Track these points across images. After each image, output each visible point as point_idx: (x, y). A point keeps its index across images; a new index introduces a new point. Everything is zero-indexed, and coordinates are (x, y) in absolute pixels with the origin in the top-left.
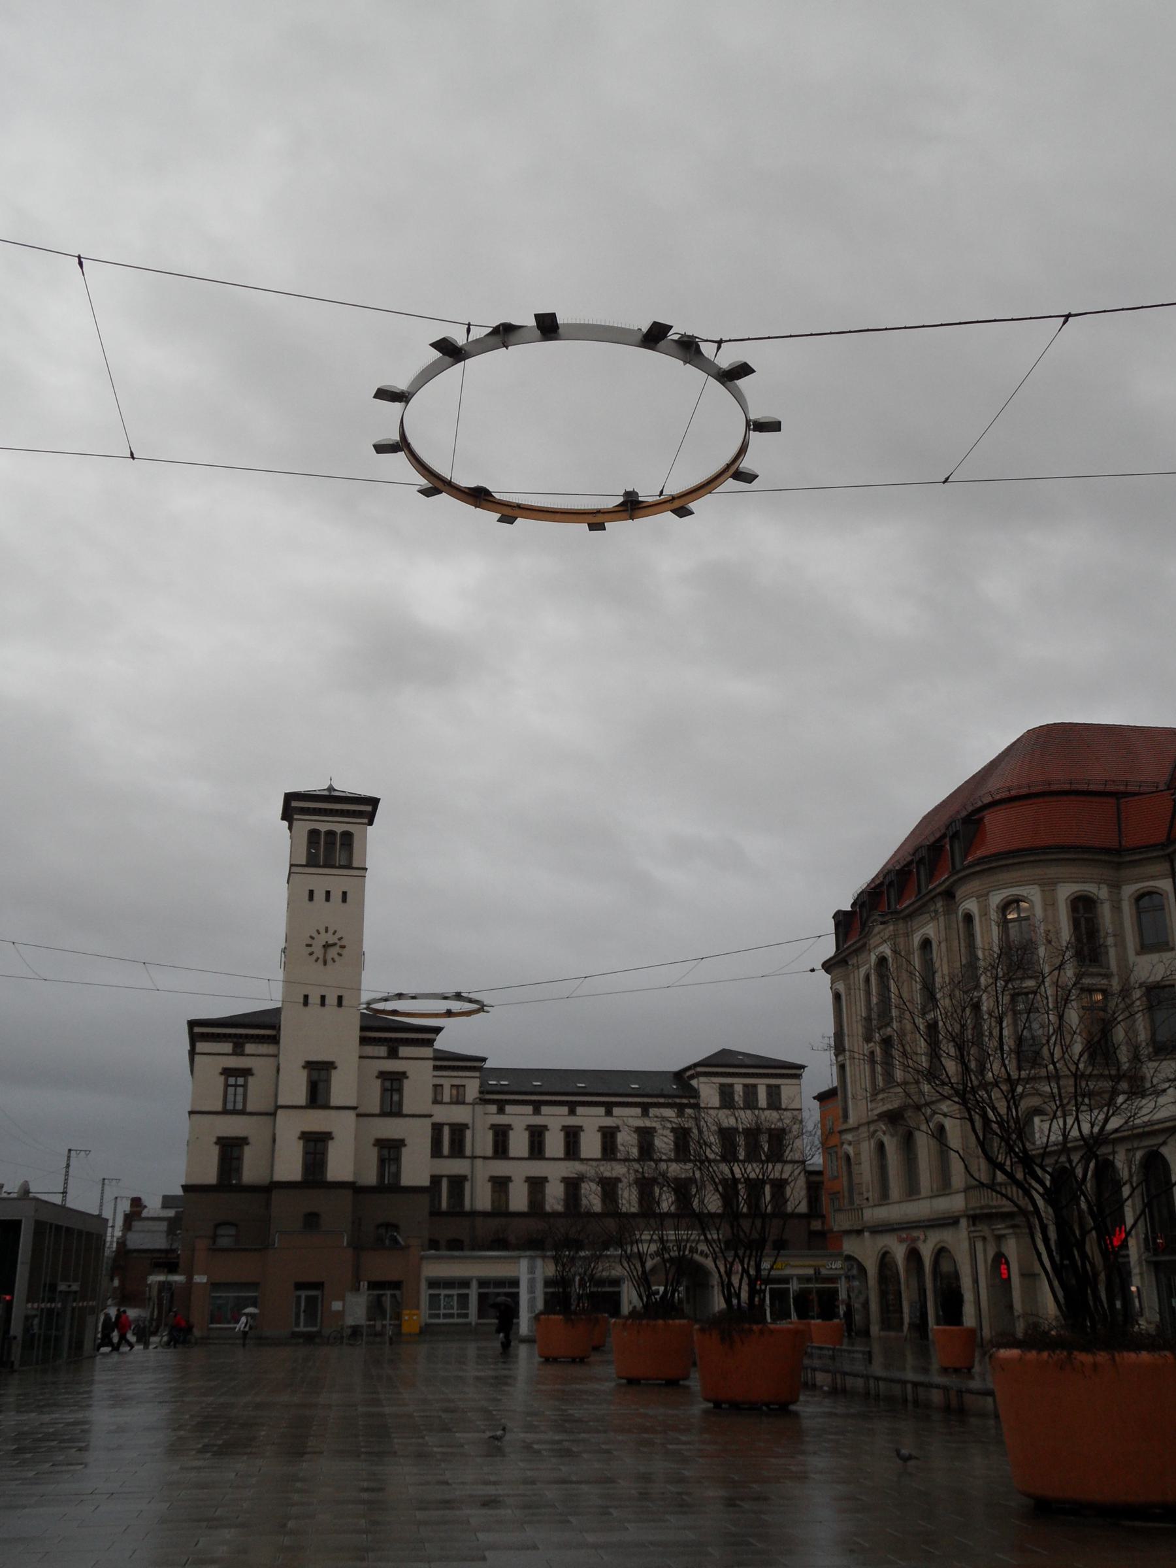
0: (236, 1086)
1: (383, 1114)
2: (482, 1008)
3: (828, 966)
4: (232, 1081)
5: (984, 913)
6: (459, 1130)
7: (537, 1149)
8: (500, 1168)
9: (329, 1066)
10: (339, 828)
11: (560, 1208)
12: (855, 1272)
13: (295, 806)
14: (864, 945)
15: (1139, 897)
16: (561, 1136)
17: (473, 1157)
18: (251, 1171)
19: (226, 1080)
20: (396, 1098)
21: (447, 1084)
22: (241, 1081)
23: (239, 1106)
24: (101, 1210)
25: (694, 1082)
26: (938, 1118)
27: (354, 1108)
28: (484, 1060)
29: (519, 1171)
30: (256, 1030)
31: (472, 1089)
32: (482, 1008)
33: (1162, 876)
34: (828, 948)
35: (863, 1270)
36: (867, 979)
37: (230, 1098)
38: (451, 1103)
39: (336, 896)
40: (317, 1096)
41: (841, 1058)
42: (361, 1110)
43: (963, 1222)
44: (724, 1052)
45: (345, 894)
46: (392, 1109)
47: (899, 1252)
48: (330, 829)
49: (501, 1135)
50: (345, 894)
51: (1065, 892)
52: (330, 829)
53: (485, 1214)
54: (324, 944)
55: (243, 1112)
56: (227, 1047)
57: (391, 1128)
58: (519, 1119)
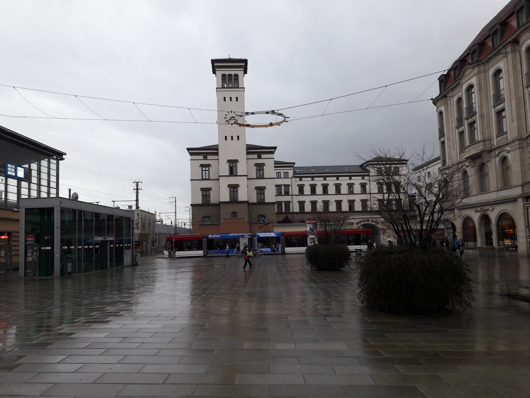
0: (205, 170)
1: (257, 178)
3: (435, 101)
4: (204, 169)
6: (287, 186)
7: (313, 191)
8: (301, 198)
9: (236, 161)
10: (233, 73)
12: (450, 226)
13: (217, 64)
14: (459, 83)
16: (321, 187)
17: (292, 195)
18: (213, 199)
19: (202, 169)
20: (261, 172)
21: (282, 172)
22: (207, 169)
23: (207, 177)
25: (368, 168)
26: (504, 154)
27: (246, 176)
28: (294, 163)
29: (308, 199)
30: (211, 151)
31: (291, 173)
34: (436, 92)
35: (454, 227)
36: (460, 100)
37: (204, 175)
38: (284, 178)
39: (234, 99)
40: (232, 172)
41: (442, 139)
42: (249, 177)
43: (520, 201)
45: (237, 98)
46: (261, 177)
47: (476, 217)
48: (230, 71)
49: (301, 188)
50: (237, 98)
52: (230, 71)
53: (297, 213)
54: (234, 120)
55: (209, 179)
56: (201, 157)
57: (260, 183)
58: (307, 182)
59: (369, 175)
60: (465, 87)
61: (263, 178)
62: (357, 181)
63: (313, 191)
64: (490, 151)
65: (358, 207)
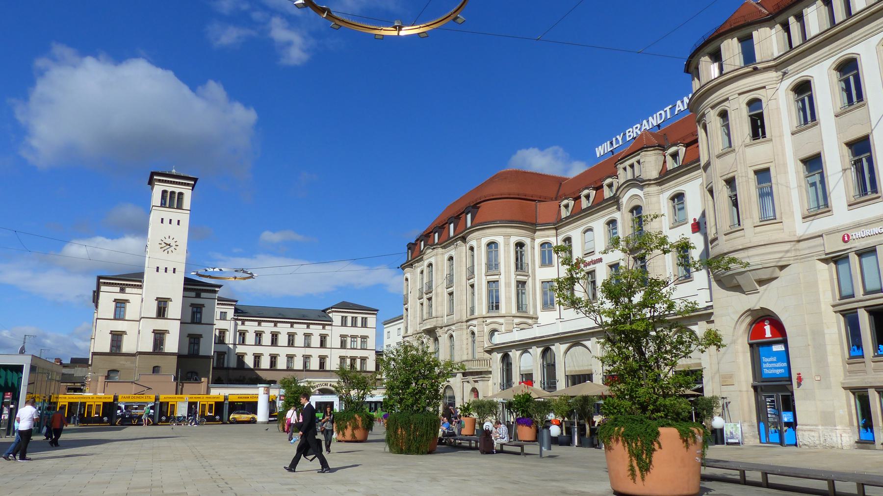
2: (251, 276)
5: (479, 247)
7: (274, 341)
11: (235, 366)
15: (543, 245)
24: (452, 355)
25: (330, 315)
32: (251, 276)
33: (553, 236)
36: (422, 272)
39: (175, 222)
40: (161, 313)
44: (344, 302)
51: (514, 240)
53: (234, 369)
56: (117, 289)
58: (251, 327)
59: (331, 325)
60: (426, 263)
61: (200, 323)
62: (316, 330)
63: (274, 341)
64: (441, 328)
65: (314, 365)
